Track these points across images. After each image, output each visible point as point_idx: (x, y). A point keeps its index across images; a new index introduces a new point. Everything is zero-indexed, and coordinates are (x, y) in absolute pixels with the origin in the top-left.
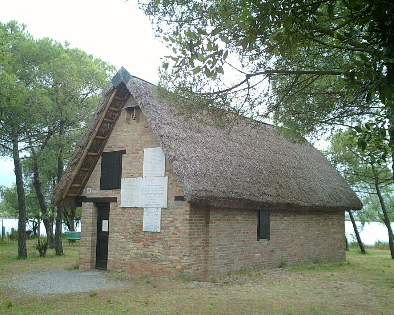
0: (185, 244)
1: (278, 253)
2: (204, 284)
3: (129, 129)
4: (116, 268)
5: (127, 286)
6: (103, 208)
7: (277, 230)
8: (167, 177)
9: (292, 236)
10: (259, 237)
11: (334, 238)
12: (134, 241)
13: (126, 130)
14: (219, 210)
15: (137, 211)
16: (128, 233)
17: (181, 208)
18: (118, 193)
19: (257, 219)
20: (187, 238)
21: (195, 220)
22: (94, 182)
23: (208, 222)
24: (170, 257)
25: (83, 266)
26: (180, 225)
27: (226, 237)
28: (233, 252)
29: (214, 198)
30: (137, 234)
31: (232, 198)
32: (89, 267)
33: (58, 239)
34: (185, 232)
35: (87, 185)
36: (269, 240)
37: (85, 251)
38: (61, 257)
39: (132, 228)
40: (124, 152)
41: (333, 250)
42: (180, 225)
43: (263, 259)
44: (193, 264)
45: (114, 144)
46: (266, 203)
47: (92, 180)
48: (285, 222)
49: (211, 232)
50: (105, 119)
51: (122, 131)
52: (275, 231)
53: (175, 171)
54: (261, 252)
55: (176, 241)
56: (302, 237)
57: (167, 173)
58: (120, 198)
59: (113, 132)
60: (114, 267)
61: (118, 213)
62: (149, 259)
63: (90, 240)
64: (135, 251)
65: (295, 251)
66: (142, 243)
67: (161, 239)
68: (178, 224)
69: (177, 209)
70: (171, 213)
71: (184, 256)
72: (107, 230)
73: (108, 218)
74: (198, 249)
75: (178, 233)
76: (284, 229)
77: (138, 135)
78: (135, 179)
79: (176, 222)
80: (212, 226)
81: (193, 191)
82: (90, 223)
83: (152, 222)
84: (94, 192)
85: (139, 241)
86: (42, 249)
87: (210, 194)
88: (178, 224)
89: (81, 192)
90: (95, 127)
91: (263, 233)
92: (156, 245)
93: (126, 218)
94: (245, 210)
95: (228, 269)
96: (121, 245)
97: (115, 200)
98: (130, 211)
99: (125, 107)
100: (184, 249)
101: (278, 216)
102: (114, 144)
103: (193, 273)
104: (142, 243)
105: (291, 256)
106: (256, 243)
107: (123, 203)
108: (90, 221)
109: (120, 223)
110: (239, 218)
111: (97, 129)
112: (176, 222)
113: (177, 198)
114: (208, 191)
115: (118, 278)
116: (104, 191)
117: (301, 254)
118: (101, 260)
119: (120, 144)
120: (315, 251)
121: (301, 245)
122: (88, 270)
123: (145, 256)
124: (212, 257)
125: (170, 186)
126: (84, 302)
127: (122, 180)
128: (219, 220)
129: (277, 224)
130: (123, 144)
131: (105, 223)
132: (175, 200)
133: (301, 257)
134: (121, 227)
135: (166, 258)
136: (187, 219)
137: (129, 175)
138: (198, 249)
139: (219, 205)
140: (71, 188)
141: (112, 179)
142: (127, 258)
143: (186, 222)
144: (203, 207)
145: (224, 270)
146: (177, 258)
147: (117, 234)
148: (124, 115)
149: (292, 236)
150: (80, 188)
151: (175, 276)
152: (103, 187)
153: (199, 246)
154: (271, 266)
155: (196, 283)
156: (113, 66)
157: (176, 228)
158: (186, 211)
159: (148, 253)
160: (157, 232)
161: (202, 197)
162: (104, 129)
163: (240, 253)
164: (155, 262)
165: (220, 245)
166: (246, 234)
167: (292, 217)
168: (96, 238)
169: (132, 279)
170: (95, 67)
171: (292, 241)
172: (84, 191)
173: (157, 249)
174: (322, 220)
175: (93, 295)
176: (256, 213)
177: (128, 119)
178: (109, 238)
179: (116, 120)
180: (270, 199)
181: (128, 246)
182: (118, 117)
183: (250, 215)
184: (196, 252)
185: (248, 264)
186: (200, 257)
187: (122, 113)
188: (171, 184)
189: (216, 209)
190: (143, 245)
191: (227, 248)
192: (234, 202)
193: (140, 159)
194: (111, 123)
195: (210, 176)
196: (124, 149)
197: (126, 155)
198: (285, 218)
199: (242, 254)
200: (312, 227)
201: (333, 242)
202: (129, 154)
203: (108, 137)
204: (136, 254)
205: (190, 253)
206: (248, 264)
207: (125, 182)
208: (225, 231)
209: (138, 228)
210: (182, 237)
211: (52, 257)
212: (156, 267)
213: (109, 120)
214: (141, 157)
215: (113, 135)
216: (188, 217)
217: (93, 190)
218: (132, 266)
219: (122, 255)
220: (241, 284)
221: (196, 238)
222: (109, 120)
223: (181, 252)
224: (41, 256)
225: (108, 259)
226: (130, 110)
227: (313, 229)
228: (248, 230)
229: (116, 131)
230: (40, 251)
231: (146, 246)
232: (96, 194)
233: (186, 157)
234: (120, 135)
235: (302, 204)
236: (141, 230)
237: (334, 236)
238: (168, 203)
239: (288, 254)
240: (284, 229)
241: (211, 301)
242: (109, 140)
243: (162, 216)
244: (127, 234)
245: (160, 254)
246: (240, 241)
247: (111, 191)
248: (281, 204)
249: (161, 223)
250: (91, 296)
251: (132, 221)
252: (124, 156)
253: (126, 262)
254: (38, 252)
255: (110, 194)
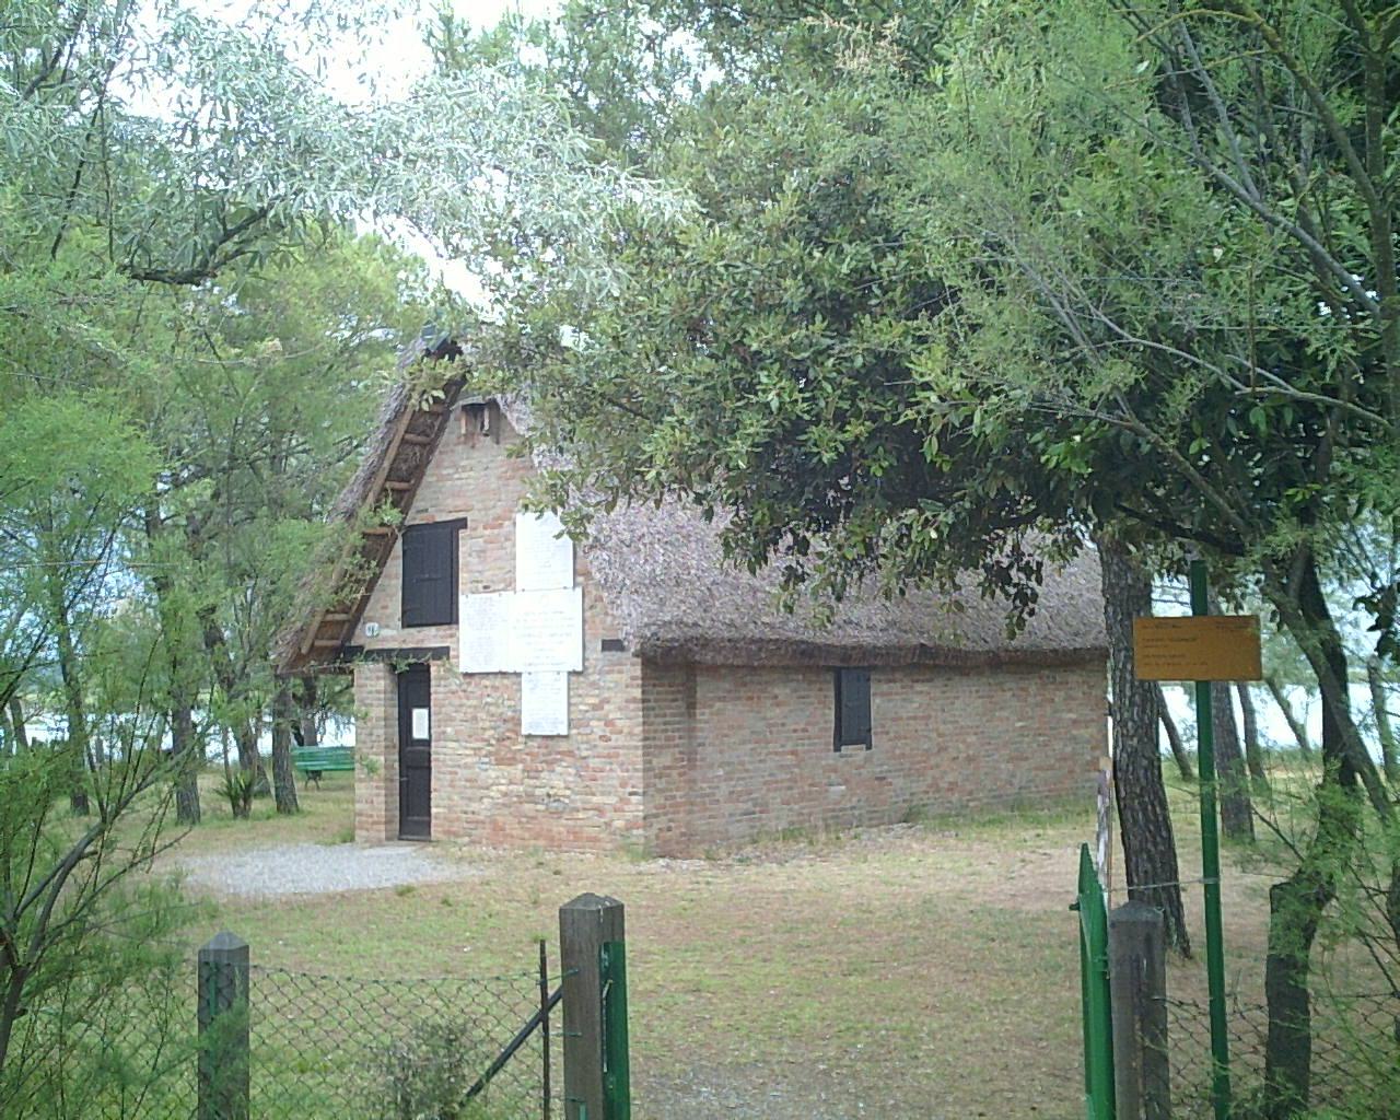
0: (634, 763)
1: (899, 782)
2: (685, 864)
3: (473, 462)
4: (456, 835)
5: (487, 873)
6: (412, 682)
7: (894, 720)
8: (579, 590)
9: (940, 735)
10: (840, 740)
11: (1074, 738)
12: (500, 762)
13: (463, 463)
14: (723, 671)
15: (506, 681)
16: (484, 740)
17: (620, 672)
18: (452, 636)
19: (832, 694)
20: (636, 748)
21: (656, 701)
22: (385, 607)
23: (691, 706)
24: (595, 799)
25: (364, 833)
26: (618, 715)
27: (744, 742)
28: (765, 783)
29: (705, 643)
30: (507, 743)
31: (753, 641)
32: (383, 835)
33: (281, 767)
34: (631, 734)
35: (366, 614)
36: (869, 748)
37: (373, 796)
38: (295, 818)
39: (494, 728)
40: (462, 523)
41: (1071, 772)
42: (618, 715)
43: (855, 799)
44: (656, 816)
45: (437, 499)
46: (854, 648)
47: (377, 601)
48: (918, 699)
49: (702, 730)
50: (408, 437)
51: (455, 466)
52: (889, 723)
53: (598, 576)
54: (846, 782)
55: (609, 756)
56: (971, 739)
57: (580, 579)
58: (457, 649)
59: (430, 470)
60: (448, 833)
61: (454, 688)
62: (540, 807)
63: (383, 758)
64: (503, 788)
65: (950, 778)
66: (520, 766)
67: (570, 753)
68: (611, 711)
69: (609, 672)
70: (593, 685)
71: (631, 794)
72: (425, 736)
73: (427, 705)
74: (669, 776)
75: (614, 737)
76: (915, 718)
77: (499, 478)
78: (495, 596)
79: (606, 707)
80: (702, 714)
81: (646, 625)
82: (378, 719)
83: (544, 710)
84: (386, 632)
85: (512, 761)
86: (240, 797)
87: (692, 632)
88: (611, 711)
89: (350, 634)
90: (382, 458)
91: (852, 729)
92: (559, 769)
93: (474, 702)
94: (797, 670)
95: (752, 827)
96: (462, 773)
97: (442, 653)
98: (486, 682)
99: (461, 403)
100: (630, 778)
101: (894, 681)
102: (437, 499)
103: (657, 837)
104: (520, 766)
105: (938, 791)
106: (832, 758)
107: (467, 660)
108: (377, 712)
109: (460, 716)
110: (781, 691)
111: (386, 464)
112: (606, 707)
113: (612, 645)
114: (686, 625)
115: (461, 859)
116: (413, 631)
117: (969, 787)
118: (412, 812)
119: (450, 503)
120: (1013, 776)
121: (970, 759)
122: (380, 844)
123: (530, 798)
124: (708, 795)
125: (588, 614)
126: (385, 906)
127: (462, 599)
128: (720, 699)
129: (889, 703)
130: (459, 502)
131: (419, 715)
132: (604, 649)
133: (971, 793)
134: (465, 727)
135: (584, 802)
136: (634, 700)
137: (480, 586)
138: (669, 776)
139: (720, 660)
140: (324, 624)
141: (434, 600)
142: (483, 808)
143: (632, 706)
144: (676, 668)
145: (741, 828)
146: (613, 800)
147: (454, 745)
148: (458, 425)
149: (940, 735)
150: (346, 626)
151: (609, 846)
152: (410, 620)
153: (669, 768)
154: (877, 818)
155: (661, 862)
156: (415, 259)
157: (609, 723)
158: (633, 678)
159: (538, 792)
160: (559, 736)
161: (673, 640)
162: (406, 461)
163: (786, 784)
164: (558, 814)
165: (729, 764)
166: (800, 734)
167: (939, 682)
168: (397, 757)
169: (499, 860)
170: (370, 270)
171: (942, 749)
172: (357, 632)
173: (559, 780)
174: (1033, 689)
175: (404, 892)
176: (830, 677)
177: (469, 436)
178: (433, 757)
179: (438, 436)
180: (867, 638)
181: (483, 774)
182: (442, 429)
183: (810, 683)
184: (661, 784)
185: (810, 814)
186: (674, 797)
187: (452, 417)
188: (591, 607)
189: (713, 670)
190: (524, 771)
191: (747, 771)
192: (760, 649)
193: (508, 544)
194: (423, 445)
195: (691, 583)
196: (461, 515)
197: (468, 532)
198: (919, 687)
199: (790, 788)
200: (1002, 709)
201: (1068, 749)
202: (475, 529)
203: (417, 485)
204: (505, 795)
205: (647, 786)
206: (810, 814)
207: (467, 604)
208: (740, 727)
209: (510, 725)
210: (623, 747)
211: (268, 818)
212: (559, 827)
213: (421, 439)
214: (510, 537)
215: (430, 477)
216: (638, 693)
217: (384, 628)
218: (497, 828)
219: (470, 799)
220: (781, 864)
221: (661, 747)
222: (421, 439)
223: (623, 785)
224: (236, 815)
225: (434, 810)
226: (474, 411)
227: (1005, 714)
228: (808, 724)
229: (438, 466)
230: (234, 800)
231: (531, 773)
232: (393, 639)
233: (627, 536)
234: (449, 477)
235: (965, 645)
236: (517, 733)
237: (1074, 732)
238: (584, 659)
239: (930, 786)
240: (915, 718)
241: (694, 895)
242: (419, 492)
243: (573, 701)
244: (479, 745)
245: (568, 792)
246: (784, 753)
247: (433, 630)
248: (900, 649)
249: (569, 712)
250: (401, 894)
251: (493, 709)
252: (462, 533)
253: (481, 818)
254: (228, 807)
255: (430, 637)
